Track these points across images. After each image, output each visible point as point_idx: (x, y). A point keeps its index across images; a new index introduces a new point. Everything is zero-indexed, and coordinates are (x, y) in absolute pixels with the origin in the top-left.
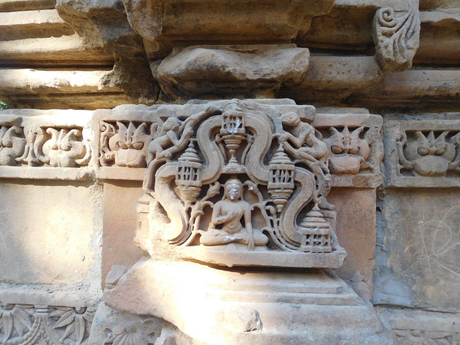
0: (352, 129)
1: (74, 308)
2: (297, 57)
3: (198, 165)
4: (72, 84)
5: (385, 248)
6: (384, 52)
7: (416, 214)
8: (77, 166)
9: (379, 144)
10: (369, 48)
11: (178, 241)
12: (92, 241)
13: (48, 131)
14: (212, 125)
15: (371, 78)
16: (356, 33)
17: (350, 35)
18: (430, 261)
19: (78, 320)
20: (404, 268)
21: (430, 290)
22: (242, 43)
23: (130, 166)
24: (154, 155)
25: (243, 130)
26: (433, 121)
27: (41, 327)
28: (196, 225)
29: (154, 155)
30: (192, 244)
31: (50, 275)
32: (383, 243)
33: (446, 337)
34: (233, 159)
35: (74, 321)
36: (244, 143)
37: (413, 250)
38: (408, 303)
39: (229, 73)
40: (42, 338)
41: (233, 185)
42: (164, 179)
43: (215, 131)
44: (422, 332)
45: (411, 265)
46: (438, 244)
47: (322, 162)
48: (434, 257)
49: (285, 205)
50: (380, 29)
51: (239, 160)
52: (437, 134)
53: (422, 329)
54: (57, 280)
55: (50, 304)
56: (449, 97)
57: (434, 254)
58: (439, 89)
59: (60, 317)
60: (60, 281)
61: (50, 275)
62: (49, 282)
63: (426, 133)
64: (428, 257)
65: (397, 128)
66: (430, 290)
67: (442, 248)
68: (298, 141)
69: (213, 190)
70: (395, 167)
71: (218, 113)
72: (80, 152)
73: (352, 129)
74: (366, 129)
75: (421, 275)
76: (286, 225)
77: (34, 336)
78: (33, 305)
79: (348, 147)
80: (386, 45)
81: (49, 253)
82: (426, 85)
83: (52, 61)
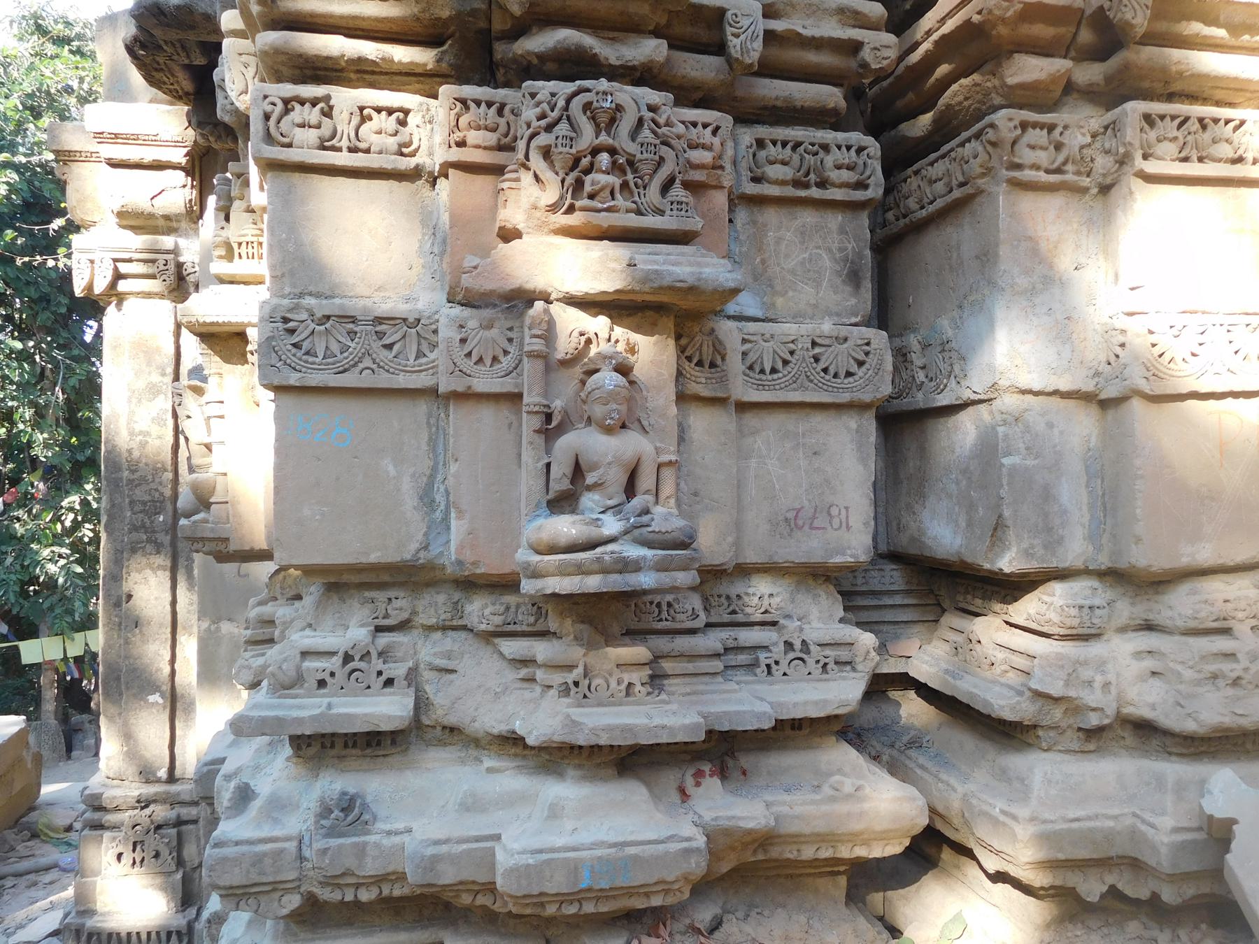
0: (705, 126)
1: (405, 320)
2: (657, 47)
3: (574, 135)
4: (396, 59)
6: (732, 51)
7: (765, 226)
8: (402, 154)
9: (730, 144)
10: (719, 48)
11: (553, 208)
13: (366, 112)
14: (585, 100)
15: (722, 77)
16: (708, 32)
17: (704, 35)
20: (756, 279)
21: (780, 301)
22: (603, 28)
23: (485, 148)
24: (529, 126)
25: (613, 106)
26: (782, 132)
28: (569, 196)
29: (529, 126)
30: (566, 213)
33: (792, 342)
34: (603, 133)
35: (404, 337)
36: (613, 120)
37: (763, 262)
38: (759, 314)
39: (595, 55)
41: (604, 158)
42: (539, 147)
43: (587, 107)
44: (772, 336)
46: (787, 256)
47: (682, 141)
49: (652, 176)
50: (729, 30)
51: (609, 134)
52: (784, 144)
56: (795, 109)
58: (785, 99)
62: (367, 294)
63: (774, 143)
64: (778, 269)
65: (747, 136)
66: (780, 301)
68: (662, 121)
69: (585, 162)
70: (746, 175)
71: (588, 90)
72: (407, 140)
73: (705, 126)
74: (718, 128)
75: (771, 286)
76: (653, 194)
79: (702, 141)
80: (734, 44)
82: (773, 94)
83: (363, 30)
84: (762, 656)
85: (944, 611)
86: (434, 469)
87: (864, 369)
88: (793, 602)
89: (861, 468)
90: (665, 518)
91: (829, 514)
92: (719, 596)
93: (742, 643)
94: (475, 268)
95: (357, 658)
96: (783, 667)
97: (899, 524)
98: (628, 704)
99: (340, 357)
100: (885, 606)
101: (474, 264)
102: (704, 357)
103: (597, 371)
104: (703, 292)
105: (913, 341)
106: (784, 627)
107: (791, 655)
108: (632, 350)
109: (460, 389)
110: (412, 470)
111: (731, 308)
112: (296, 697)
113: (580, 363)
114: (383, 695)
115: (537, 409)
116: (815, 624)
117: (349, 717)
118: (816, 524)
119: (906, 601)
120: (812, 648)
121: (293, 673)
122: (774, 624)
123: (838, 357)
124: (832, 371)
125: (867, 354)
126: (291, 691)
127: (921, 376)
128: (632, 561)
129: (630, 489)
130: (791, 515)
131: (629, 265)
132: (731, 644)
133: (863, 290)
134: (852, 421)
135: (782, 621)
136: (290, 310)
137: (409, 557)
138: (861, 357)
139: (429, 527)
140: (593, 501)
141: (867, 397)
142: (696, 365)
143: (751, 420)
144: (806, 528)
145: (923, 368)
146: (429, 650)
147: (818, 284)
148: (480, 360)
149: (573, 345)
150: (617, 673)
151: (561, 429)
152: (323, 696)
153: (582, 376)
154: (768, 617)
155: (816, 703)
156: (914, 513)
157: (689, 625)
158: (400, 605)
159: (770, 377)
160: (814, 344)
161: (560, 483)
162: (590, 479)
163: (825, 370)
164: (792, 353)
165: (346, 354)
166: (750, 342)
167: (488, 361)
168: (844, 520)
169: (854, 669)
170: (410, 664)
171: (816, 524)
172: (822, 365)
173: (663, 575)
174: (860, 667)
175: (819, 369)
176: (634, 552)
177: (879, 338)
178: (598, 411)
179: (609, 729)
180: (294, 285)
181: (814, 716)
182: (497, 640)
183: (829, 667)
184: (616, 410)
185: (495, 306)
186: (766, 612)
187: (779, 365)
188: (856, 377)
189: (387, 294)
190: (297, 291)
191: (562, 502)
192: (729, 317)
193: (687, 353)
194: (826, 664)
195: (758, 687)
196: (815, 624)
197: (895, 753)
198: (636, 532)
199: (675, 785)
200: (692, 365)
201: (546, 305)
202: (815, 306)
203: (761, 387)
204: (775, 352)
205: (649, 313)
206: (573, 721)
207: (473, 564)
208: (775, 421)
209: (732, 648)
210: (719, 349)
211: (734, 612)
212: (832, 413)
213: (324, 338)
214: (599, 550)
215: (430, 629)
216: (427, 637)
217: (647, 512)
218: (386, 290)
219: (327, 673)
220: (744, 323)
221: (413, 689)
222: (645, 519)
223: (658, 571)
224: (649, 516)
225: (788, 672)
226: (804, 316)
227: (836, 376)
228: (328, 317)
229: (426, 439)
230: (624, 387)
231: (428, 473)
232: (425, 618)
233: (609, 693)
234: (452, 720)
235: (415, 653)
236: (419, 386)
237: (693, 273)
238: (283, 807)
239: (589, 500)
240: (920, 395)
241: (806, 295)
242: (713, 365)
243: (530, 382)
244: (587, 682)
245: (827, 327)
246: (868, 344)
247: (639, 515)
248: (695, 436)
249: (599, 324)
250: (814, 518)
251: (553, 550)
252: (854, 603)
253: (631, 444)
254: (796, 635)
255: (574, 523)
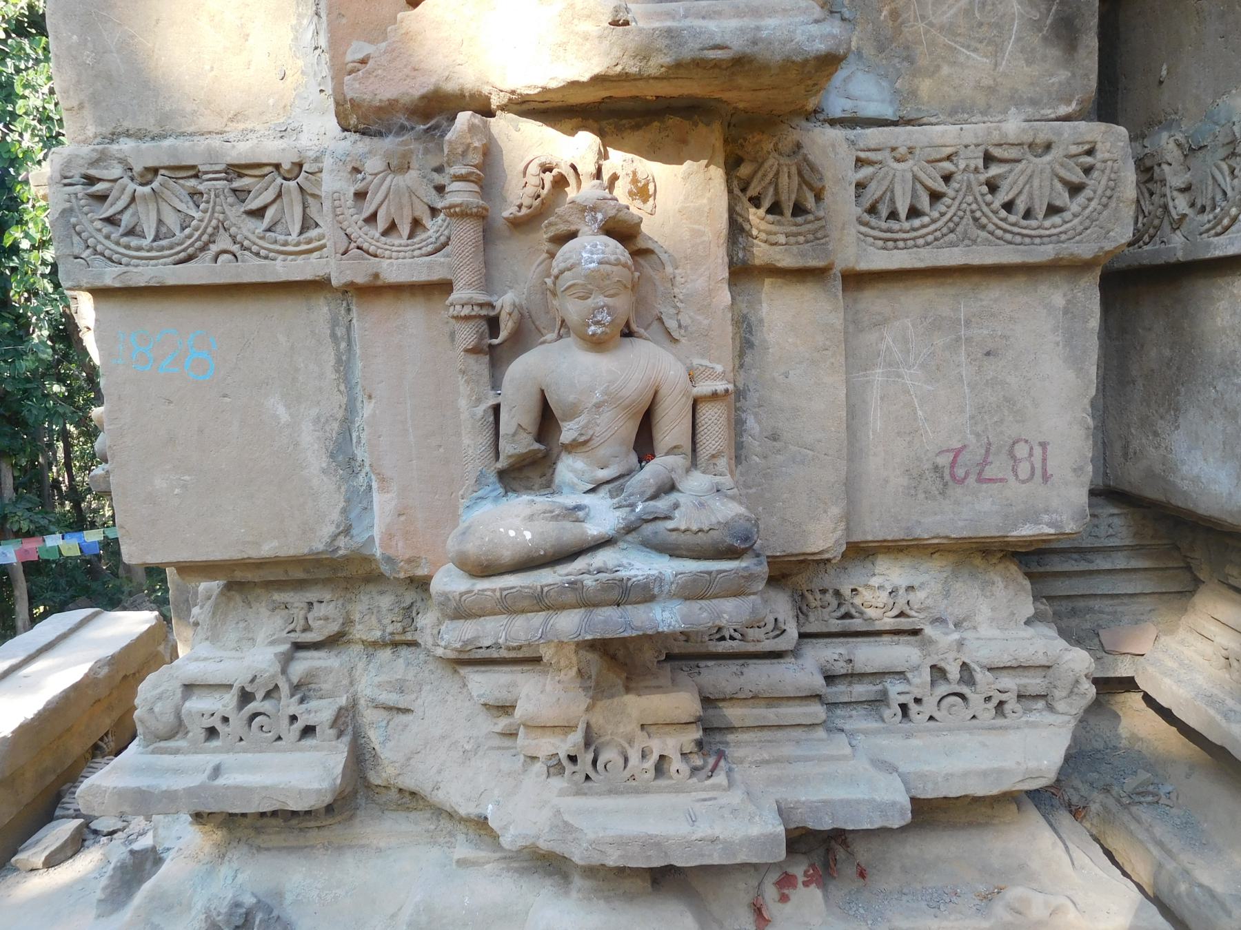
1: (277, 166)
5: (847, 15)
12: (296, 39)
18: (925, 34)
19: (289, 191)
20: (881, 49)
21: (925, 86)
27: (218, 208)
31: (220, 114)
32: (843, 6)
33: (949, 158)
35: (279, 195)
37: (895, 14)
38: (888, 112)
40: (221, 230)
45: (892, 42)
48: (931, 24)
53: (909, 144)
54: (234, 124)
55: (230, 160)
57: (932, 18)
59: (249, 192)
60: (241, 126)
61: (220, 114)
62: (219, 128)
64: (921, 26)
66: (925, 86)
67: (945, 8)
75: (910, 59)
77: (206, 228)
78: (193, 167)
81: (212, 68)
84: (895, 689)
85: (1197, 582)
86: (350, 410)
87: (1081, 199)
88: (947, 595)
89: (1070, 375)
90: (705, 502)
91: (1012, 456)
92: (824, 591)
93: (860, 667)
94: (363, 62)
95: (260, 695)
96: (929, 707)
97: (1126, 447)
98: (660, 791)
99: (180, 235)
100: (1098, 572)
101: (360, 56)
102: (784, 197)
103: (573, 235)
104: (764, 68)
105: (1167, 144)
106: (931, 642)
107: (943, 689)
108: (642, 192)
109: (360, 280)
110: (314, 411)
111: (837, 106)
112: (176, 751)
113: (545, 218)
114: (301, 750)
115: (466, 311)
116: (985, 631)
117: (244, 791)
118: (989, 472)
119: (1134, 564)
120: (980, 676)
121: (170, 718)
122: (915, 632)
123: (1032, 181)
124: (1021, 206)
125: (1088, 170)
126: (171, 744)
127: (1181, 204)
128: (636, 586)
129: (644, 443)
130: (944, 460)
131: (615, 23)
132: (841, 668)
133: (1082, 53)
134: (1056, 294)
135: (929, 631)
136: (94, 163)
137: (321, 547)
138: (1077, 177)
139: (348, 501)
140: (574, 471)
141: (1086, 250)
142: (769, 211)
143: (873, 301)
144: (971, 480)
145: (1186, 189)
146: (373, 678)
147: (997, 49)
148: (392, 228)
149: (530, 190)
150: (642, 740)
151: (521, 339)
152: (215, 751)
153: (547, 246)
154: (904, 623)
155: (985, 774)
156: (1156, 434)
157: (768, 645)
158: (326, 614)
159: (907, 225)
160: (989, 159)
161: (517, 443)
162: (568, 432)
163: (1009, 206)
164: (947, 178)
165: (187, 231)
166: (870, 163)
167: (405, 229)
168: (1038, 465)
169: (1050, 708)
170: (343, 701)
171: (989, 472)
172: (1003, 197)
173: (696, 606)
174: (1061, 706)
175: (997, 204)
176: (640, 566)
177: (1113, 140)
178: (573, 309)
179: (621, 842)
180: (100, 122)
181: (980, 792)
182: (464, 671)
183: (1007, 708)
184: (608, 307)
185: (403, 128)
186: (902, 614)
187: (884, 211)
188: (1067, 215)
189: (249, 125)
190: (106, 130)
191: (527, 471)
192: (833, 122)
193: (752, 191)
194: (1001, 703)
195: (884, 741)
196: (985, 631)
197: (1111, 802)
198: (648, 529)
199: (746, 899)
200: (761, 212)
201: (478, 119)
202: (991, 90)
203: (889, 243)
204: (915, 178)
205: (672, 121)
206: (566, 823)
207: (409, 561)
208: (915, 302)
209: (845, 675)
210: (811, 181)
211: (848, 616)
212: (1021, 280)
213: (152, 207)
214: (580, 564)
215: (376, 645)
216: (370, 656)
217: (672, 488)
218: (246, 118)
219: (217, 717)
220: (859, 130)
221: (346, 739)
222: (662, 504)
223: (687, 599)
224: (674, 497)
225: (935, 715)
226: (971, 112)
227: (1028, 215)
228: (155, 171)
229: (332, 362)
230: (618, 263)
231: (340, 414)
232: (359, 632)
233: (627, 774)
234: (408, 783)
235: (352, 684)
236: (309, 277)
237: (742, 30)
238: (170, 908)
239: (569, 469)
240: (1177, 239)
241: (975, 67)
242: (799, 210)
243: (457, 264)
244: (590, 756)
245: (1013, 126)
246: (1090, 152)
247: (654, 497)
248: (771, 337)
249: (577, 148)
250: (985, 462)
251: (485, 569)
252: (1048, 569)
253: (645, 365)
254: (951, 655)
255: (531, 518)
